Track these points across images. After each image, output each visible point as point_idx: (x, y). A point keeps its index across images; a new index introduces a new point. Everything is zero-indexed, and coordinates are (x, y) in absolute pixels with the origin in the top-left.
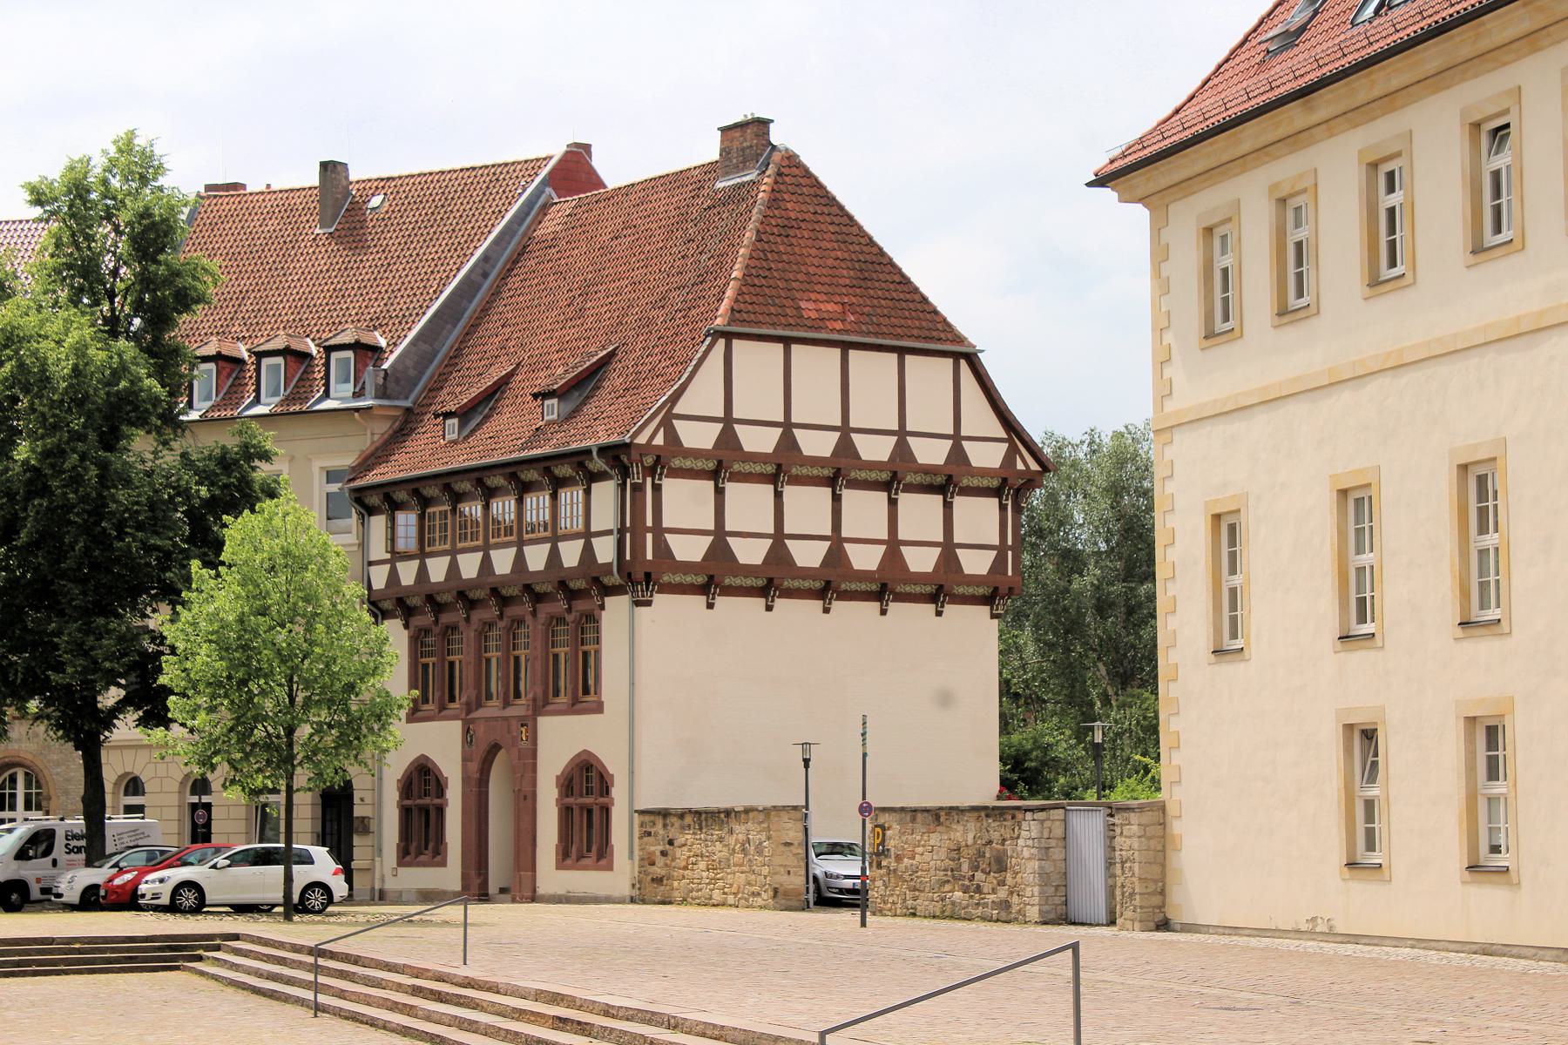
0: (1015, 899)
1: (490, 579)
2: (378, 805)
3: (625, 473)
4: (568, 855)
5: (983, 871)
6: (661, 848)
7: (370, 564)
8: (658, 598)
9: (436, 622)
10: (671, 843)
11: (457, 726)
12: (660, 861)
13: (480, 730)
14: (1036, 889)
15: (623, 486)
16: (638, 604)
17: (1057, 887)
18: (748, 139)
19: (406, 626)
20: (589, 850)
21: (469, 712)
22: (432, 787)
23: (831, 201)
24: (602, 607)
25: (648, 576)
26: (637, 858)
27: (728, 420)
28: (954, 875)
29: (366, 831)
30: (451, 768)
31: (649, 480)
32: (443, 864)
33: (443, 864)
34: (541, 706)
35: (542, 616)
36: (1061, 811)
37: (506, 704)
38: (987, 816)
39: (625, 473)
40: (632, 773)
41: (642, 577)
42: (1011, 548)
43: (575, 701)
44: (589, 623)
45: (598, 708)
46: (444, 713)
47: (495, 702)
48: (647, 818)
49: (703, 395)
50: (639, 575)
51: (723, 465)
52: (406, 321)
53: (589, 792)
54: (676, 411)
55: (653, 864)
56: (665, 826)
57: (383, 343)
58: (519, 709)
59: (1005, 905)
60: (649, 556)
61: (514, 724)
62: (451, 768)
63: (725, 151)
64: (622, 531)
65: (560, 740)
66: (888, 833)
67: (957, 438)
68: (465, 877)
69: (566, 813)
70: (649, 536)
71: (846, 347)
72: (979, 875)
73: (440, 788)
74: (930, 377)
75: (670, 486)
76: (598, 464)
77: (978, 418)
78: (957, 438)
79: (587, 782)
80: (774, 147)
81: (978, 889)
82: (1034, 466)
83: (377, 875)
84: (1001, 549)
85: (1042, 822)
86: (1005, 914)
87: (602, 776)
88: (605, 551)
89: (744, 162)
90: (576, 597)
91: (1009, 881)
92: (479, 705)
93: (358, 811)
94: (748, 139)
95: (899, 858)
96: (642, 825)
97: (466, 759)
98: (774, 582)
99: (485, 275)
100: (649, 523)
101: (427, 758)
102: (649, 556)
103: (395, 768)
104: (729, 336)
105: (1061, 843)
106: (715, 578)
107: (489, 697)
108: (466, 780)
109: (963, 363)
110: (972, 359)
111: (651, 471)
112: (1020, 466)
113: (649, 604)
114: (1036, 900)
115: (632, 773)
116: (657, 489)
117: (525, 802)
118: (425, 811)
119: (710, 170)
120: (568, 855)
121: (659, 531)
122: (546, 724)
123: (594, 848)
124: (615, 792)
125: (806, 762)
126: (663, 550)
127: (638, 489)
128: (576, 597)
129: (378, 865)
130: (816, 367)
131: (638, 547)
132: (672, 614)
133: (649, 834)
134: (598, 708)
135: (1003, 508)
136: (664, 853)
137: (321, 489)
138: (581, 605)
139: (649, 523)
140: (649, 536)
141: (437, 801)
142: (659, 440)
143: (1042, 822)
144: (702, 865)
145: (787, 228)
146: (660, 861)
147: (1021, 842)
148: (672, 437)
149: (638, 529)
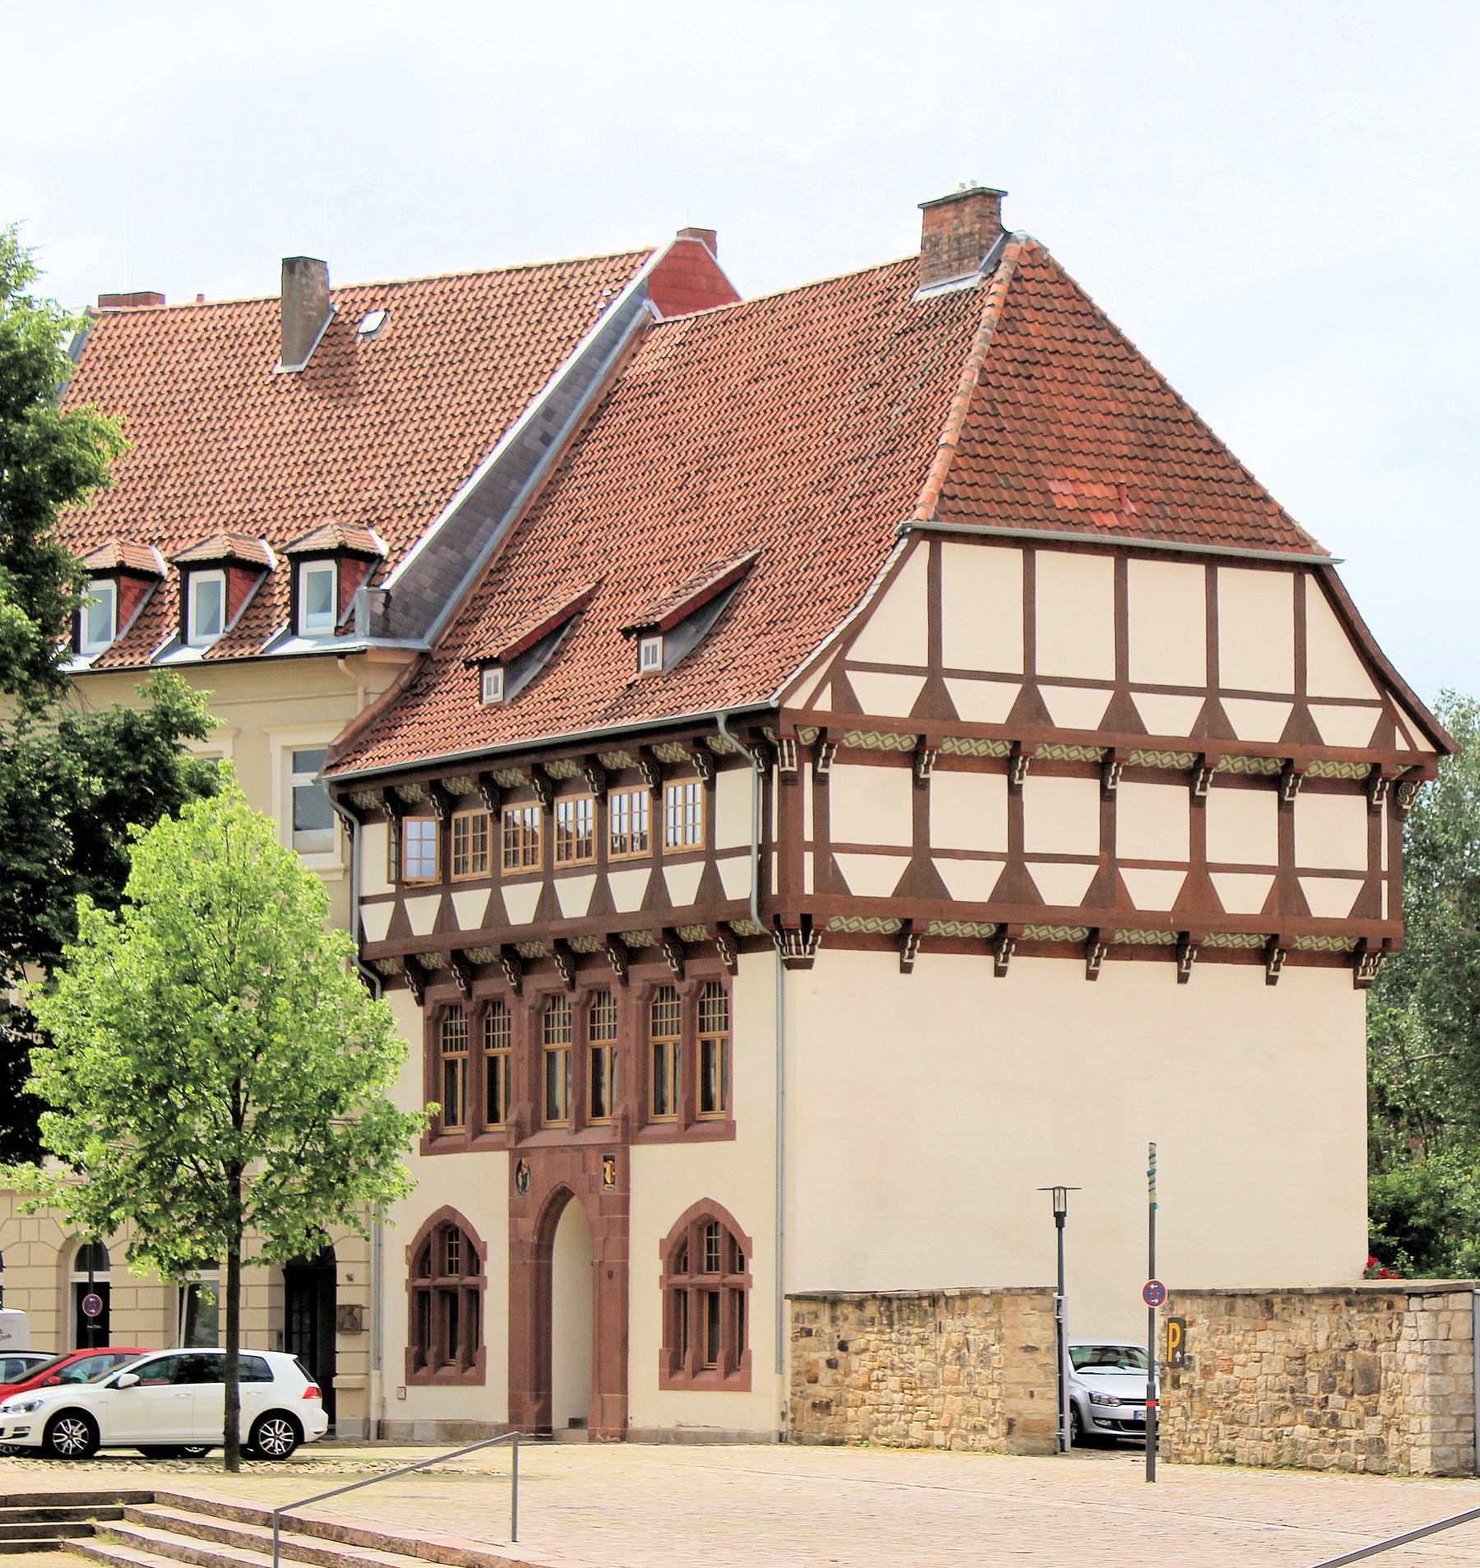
0: (1393, 1437)
1: (555, 926)
2: (375, 1285)
3: (770, 755)
4: (678, 1366)
5: (1342, 1392)
6: (827, 1355)
7: (363, 901)
8: (822, 956)
9: (469, 993)
10: (843, 1347)
11: (499, 1162)
12: (826, 1375)
13: (538, 1166)
14: (1427, 1422)
15: (766, 777)
16: (790, 964)
17: (1460, 1418)
18: (967, 221)
19: (421, 1001)
20: (712, 1359)
21: (520, 1137)
22: (462, 1258)
23: (1100, 322)
24: (733, 970)
25: (806, 920)
26: (788, 1371)
27: (935, 672)
28: (1295, 1397)
29: (356, 1328)
30: (493, 1229)
31: (808, 767)
32: (480, 1380)
33: (480, 1380)
34: (635, 1129)
35: (637, 984)
36: (1468, 1296)
37: (580, 1125)
38: (1349, 1304)
39: (770, 755)
40: (780, 1235)
41: (795, 925)
42: (1386, 876)
43: (690, 1121)
44: (717, 988)
45: (728, 1132)
46: (481, 1139)
47: (563, 1123)
48: (805, 1307)
49: (894, 631)
50: (792, 919)
51: (925, 745)
52: (419, 513)
53: (712, 1265)
54: (851, 656)
55: (814, 1380)
56: (834, 1320)
57: (383, 548)
58: (601, 1132)
59: (1378, 1446)
60: (809, 889)
61: (593, 1158)
62: (493, 1229)
63: (930, 243)
64: (764, 849)
65: (665, 1182)
66: (1190, 1331)
67: (1300, 699)
68: (514, 1402)
69: (676, 1298)
70: (809, 858)
71: (1123, 553)
72: (1336, 1399)
73: (475, 1260)
74: (1257, 601)
75: (840, 775)
76: (726, 741)
77: (1335, 669)
78: (1300, 699)
79: (709, 1250)
80: (1008, 235)
81: (1334, 1421)
82: (1423, 745)
83: (374, 1399)
84: (1371, 878)
85: (1436, 1313)
86: (1376, 1461)
87: (733, 1240)
88: (738, 880)
89: (959, 259)
90: (693, 952)
91: (1384, 1407)
92: (537, 1127)
93: (343, 1296)
94: (967, 221)
95: (1207, 1372)
96: (797, 1318)
97: (515, 1213)
98: (1098, 936)
99: (547, 440)
100: (809, 835)
101: (454, 1212)
102: (809, 889)
103: (403, 1228)
104: (936, 537)
105: (1466, 1348)
106: (911, 925)
107: (552, 1113)
108: (515, 1247)
109: (1310, 580)
110: (1323, 574)
111: (812, 752)
112: (1401, 745)
113: (807, 964)
114: (1427, 1439)
115: (780, 1235)
116: (821, 781)
117: (610, 1279)
118: (450, 1295)
119: (906, 270)
120: (678, 1366)
121: (824, 847)
122: (643, 1156)
123: (721, 1355)
124: (753, 1265)
125: (1060, 1217)
126: (831, 879)
127: (790, 781)
128: (693, 952)
129: (375, 1382)
130: (1075, 585)
131: (793, 873)
132: (844, 976)
133: (809, 1333)
134: (728, 1132)
135: (1373, 811)
136: (832, 1364)
137: (284, 781)
138: (699, 967)
139: (809, 835)
140: (809, 858)
141: (469, 1280)
142: (824, 704)
143: (1436, 1313)
144: (893, 1382)
145: (1029, 365)
146: (826, 1375)
147: (1402, 1345)
148: (845, 699)
149: (790, 847)
